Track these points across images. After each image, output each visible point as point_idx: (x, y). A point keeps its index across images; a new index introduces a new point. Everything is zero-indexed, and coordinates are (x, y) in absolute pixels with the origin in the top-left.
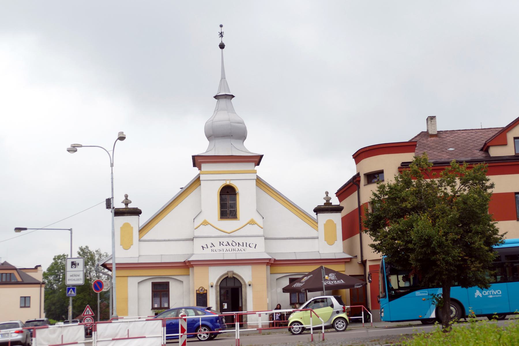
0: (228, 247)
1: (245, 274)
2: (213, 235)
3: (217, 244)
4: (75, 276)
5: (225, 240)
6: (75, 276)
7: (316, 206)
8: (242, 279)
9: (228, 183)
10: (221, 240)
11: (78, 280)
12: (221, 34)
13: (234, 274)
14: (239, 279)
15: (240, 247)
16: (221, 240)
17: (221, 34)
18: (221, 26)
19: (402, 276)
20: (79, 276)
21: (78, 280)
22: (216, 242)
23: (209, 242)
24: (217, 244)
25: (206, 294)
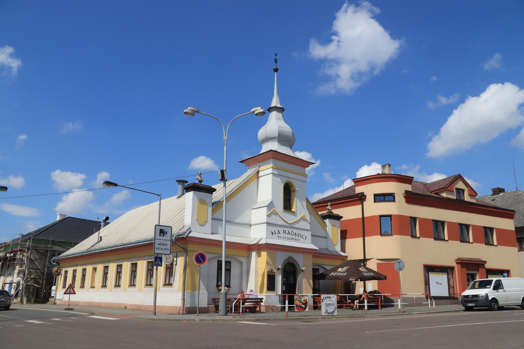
0: (289, 236)
1: (299, 259)
2: (279, 223)
3: (282, 232)
4: (163, 245)
5: (287, 230)
6: (163, 245)
7: (456, 258)
8: (298, 265)
9: (290, 180)
10: (285, 229)
11: (166, 249)
12: (276, 61)
13: (294, 260)
14: (295, 263)
15: (297, 237)
16: (285, 229)
17: (276, 61)
18: (276, 55)
19: (15, 70)
20: (166, 245)
21: (166, 249)
22: (281, 230)
23: (276, 229)
24: (282, 232)
25: (274, 276)
